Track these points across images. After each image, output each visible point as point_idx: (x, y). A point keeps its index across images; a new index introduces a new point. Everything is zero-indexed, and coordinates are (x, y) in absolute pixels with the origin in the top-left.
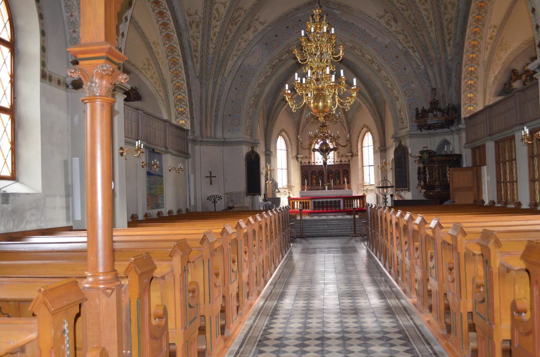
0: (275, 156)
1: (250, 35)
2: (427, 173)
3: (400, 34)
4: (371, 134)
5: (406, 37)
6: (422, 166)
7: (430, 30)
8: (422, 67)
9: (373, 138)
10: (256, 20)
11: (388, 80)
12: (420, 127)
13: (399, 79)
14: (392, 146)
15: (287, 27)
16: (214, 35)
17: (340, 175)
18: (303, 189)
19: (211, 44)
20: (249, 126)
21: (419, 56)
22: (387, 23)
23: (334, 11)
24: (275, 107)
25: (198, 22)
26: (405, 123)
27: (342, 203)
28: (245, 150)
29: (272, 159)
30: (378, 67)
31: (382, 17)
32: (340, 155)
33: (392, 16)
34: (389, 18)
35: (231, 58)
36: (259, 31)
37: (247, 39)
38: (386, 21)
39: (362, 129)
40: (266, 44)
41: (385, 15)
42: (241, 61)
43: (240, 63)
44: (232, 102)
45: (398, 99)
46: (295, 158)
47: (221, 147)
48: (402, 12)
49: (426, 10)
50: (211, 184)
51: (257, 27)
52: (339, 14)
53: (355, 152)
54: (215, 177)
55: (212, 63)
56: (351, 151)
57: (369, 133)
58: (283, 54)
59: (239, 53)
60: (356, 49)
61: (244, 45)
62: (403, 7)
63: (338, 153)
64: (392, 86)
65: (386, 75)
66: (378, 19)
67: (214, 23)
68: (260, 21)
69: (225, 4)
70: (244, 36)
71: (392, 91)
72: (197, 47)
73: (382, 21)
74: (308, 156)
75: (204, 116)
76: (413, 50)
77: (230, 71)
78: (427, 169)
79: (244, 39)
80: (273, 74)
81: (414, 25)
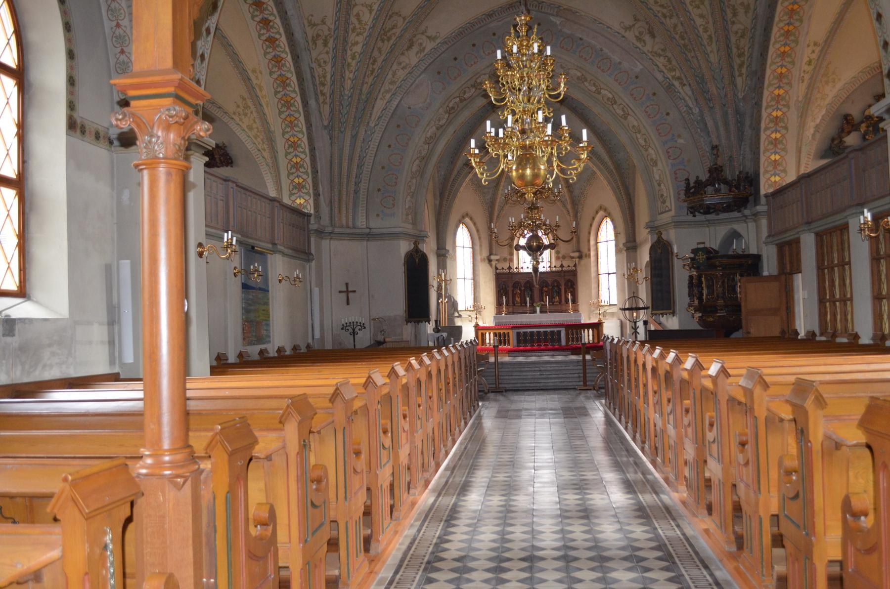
0: (454, 258)
1: (412, 58)
2: (704, 285)
3: (660, 55)
4: (612, 221)
5: (669, 61)
6: (695, 273)
7: (709, 49)
8: (696, 111)
9: (615, 228)
10: (422, 33)
11: (639, 132)
12: (693, 210)
13: (658, 130)
14: (646, 241)
15: (474, 45)
16: (353, 58)
17: (560, 290)
18: (499, 312)
19: (347, 72)
20: (410, 207)
21: (690, 93)
22: (638, 39)
23: (551, 18)
24: (453, 177)
25: (326, 37)
26: (668, 204)
27: (563, 334)
28: (404, 247)
29: (449, 262)
30: (623, 111)
31: (630, 28)
32: (560, 255)
33: (647, 27)
34: (642, 29)
35: (380, 96)
36: (427, 51)
37: (407, 65)
38: (637, 34)
39: (597, 212)
40: (439, 73)
41: (634, 25)
42: (397, 101)
43: (396, 103)
44: (383, 168)
45: (655, 164)
46: (487, 261)
47: (365, 243)
48: (663, 19)
49: (701, 16)
50: (348, 303)
51: (424, 45)
52: (558, 22)
53: (585, 251)
54: (354, 291)
55: (349, 104)
56: (578, 248)
57: (608, 220)
58: (467, 89)
59: (393, 87)
60: (586, 80)
61: (401, 74)
62: (665, 11)
63: (557, 252)
64: (645, 141)
65: (635, 123)
66: (622, 32)
67: (352, 37)
68: (429, 34)
69: (371, 7)
70: (403, 59)
71: (646, 150)
72: (324, 77)
73: (630, 35)
74: (508, 257)
75: (336, 191)
76: (681, 83)
77: (380, 117)
78: (703, 279)
79: (402, 65)
80: (449, 122)
81: (683, 42)
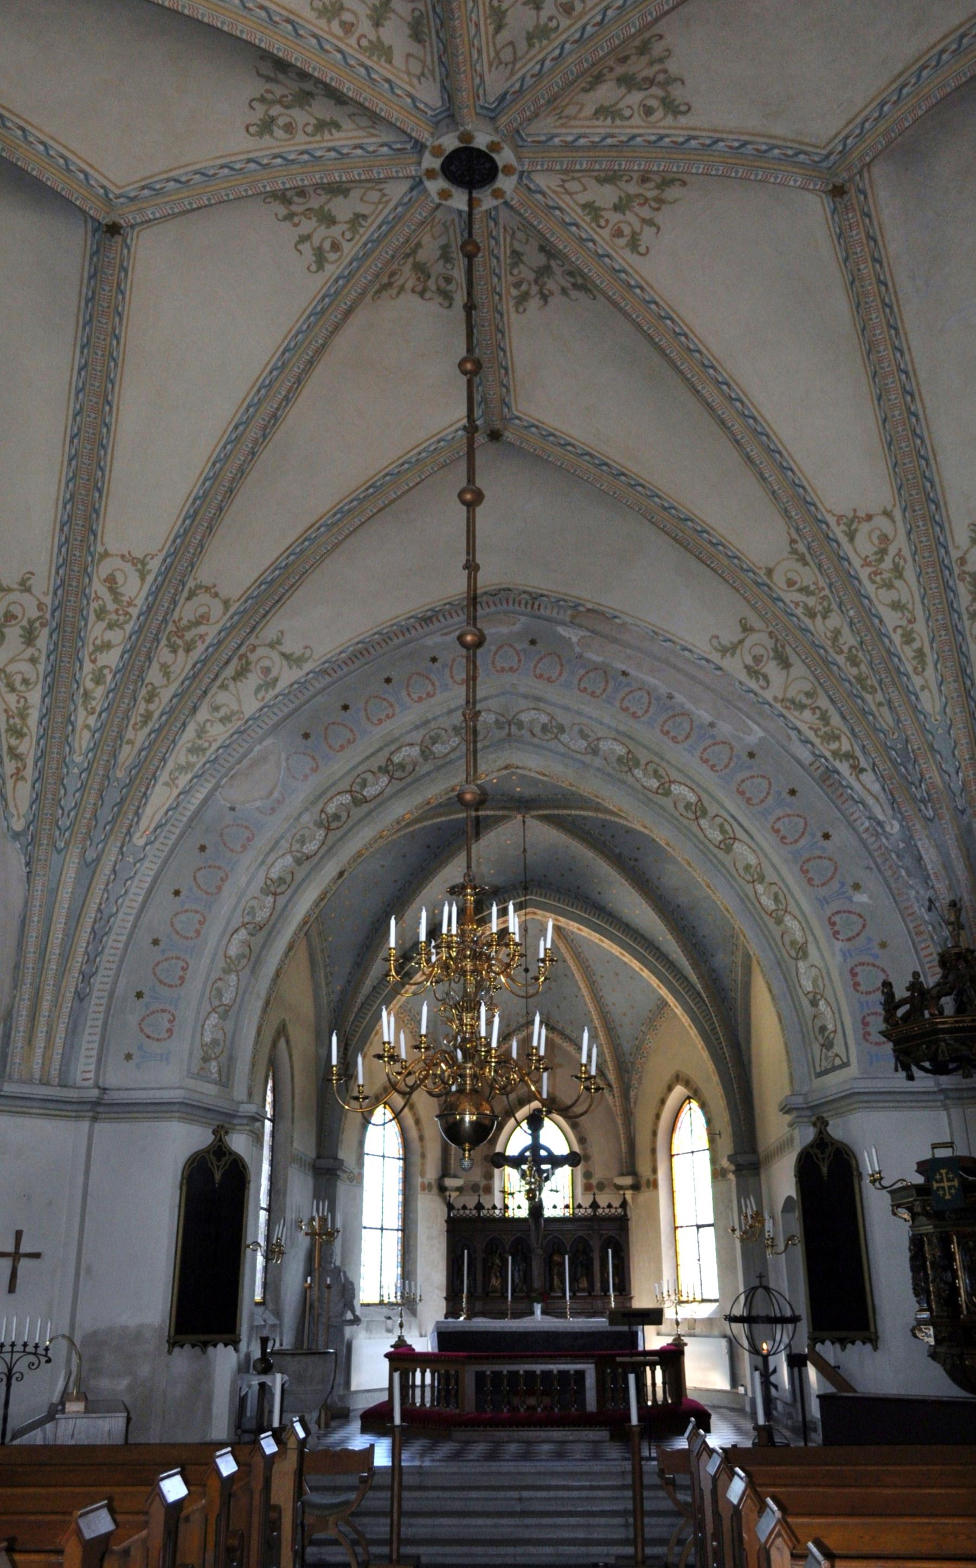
0: (357, 1179)
1: (245, 698)
2: (958, 1264)
3: (802, 707)
4: (703, 1106)
5: (825, 718)
6: (929, 1229)
7: (917, 681)
8: (894, 828)
9: (709, 1122)
10: (272, 646)
11: (762, 879)
12: (906, 1059)
13: (804, 872)
14: (782, 1148)
15: (388, 681)
16: (98, 680)
17: (591, 1260)
18: (452, 1312)
19: (82, 713)
20: (215, 1042)
21: (876, 788)
22: (753, 672)
23: (560, 630)
24: (360, 999)
25: (31, 623)
26: (838, 1048)
27: (590, 1381)
28: (183, 1140)
29: (342, 1189)
30: (722, 830)
31: (730, 650)
32: (594, 1182)
33: (770, 644)
34: (759, 651)
35: (164, 777)
36: (281, 685)
37: (233, 713)
38: (749, 661)
39: (670, 1089)
40: (306, 736)
41: (741, 642)
42: (205, 791)
43: (201, 796)
44: (156, 942)
45: (802, 952)
46: (435, 1190)
47: (85, 1125)
48: (807, 621)
49: (897, 606)
50: (12, 1289)
51: (274, 673)
52: (575, 639)
54: (37, 1256)
55: (83, 787)
56: (632, 1165)
57: (694, 1104)
58: (369, 776)
59: (198, 761)
60: (637, 764)
61: (219, 733)
62: (811, 601)
63: (587, 1175)
64: (776, 899)
65: (752, 860)
66: (716, 657)
67: (96, 631)
68: (287, 648)
69: (144, 564)
70: (222, 698)
71: (779, 922)
72: (23, 716)
73: (734, 665)
74: (483, 1183)
75: (26, 991)
76: (853, 767)
77: (160, 826)
78: (954, 1247)
79: (222, 713)
80: (328, 850)
81: (855, 671)
